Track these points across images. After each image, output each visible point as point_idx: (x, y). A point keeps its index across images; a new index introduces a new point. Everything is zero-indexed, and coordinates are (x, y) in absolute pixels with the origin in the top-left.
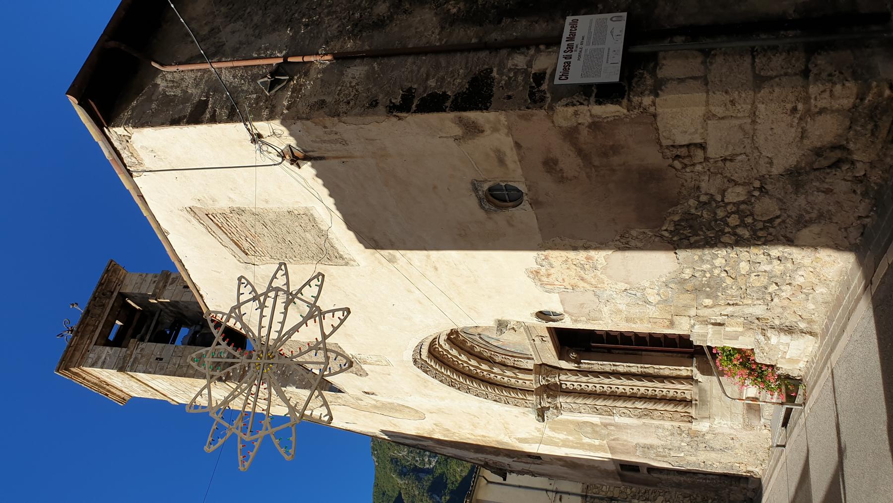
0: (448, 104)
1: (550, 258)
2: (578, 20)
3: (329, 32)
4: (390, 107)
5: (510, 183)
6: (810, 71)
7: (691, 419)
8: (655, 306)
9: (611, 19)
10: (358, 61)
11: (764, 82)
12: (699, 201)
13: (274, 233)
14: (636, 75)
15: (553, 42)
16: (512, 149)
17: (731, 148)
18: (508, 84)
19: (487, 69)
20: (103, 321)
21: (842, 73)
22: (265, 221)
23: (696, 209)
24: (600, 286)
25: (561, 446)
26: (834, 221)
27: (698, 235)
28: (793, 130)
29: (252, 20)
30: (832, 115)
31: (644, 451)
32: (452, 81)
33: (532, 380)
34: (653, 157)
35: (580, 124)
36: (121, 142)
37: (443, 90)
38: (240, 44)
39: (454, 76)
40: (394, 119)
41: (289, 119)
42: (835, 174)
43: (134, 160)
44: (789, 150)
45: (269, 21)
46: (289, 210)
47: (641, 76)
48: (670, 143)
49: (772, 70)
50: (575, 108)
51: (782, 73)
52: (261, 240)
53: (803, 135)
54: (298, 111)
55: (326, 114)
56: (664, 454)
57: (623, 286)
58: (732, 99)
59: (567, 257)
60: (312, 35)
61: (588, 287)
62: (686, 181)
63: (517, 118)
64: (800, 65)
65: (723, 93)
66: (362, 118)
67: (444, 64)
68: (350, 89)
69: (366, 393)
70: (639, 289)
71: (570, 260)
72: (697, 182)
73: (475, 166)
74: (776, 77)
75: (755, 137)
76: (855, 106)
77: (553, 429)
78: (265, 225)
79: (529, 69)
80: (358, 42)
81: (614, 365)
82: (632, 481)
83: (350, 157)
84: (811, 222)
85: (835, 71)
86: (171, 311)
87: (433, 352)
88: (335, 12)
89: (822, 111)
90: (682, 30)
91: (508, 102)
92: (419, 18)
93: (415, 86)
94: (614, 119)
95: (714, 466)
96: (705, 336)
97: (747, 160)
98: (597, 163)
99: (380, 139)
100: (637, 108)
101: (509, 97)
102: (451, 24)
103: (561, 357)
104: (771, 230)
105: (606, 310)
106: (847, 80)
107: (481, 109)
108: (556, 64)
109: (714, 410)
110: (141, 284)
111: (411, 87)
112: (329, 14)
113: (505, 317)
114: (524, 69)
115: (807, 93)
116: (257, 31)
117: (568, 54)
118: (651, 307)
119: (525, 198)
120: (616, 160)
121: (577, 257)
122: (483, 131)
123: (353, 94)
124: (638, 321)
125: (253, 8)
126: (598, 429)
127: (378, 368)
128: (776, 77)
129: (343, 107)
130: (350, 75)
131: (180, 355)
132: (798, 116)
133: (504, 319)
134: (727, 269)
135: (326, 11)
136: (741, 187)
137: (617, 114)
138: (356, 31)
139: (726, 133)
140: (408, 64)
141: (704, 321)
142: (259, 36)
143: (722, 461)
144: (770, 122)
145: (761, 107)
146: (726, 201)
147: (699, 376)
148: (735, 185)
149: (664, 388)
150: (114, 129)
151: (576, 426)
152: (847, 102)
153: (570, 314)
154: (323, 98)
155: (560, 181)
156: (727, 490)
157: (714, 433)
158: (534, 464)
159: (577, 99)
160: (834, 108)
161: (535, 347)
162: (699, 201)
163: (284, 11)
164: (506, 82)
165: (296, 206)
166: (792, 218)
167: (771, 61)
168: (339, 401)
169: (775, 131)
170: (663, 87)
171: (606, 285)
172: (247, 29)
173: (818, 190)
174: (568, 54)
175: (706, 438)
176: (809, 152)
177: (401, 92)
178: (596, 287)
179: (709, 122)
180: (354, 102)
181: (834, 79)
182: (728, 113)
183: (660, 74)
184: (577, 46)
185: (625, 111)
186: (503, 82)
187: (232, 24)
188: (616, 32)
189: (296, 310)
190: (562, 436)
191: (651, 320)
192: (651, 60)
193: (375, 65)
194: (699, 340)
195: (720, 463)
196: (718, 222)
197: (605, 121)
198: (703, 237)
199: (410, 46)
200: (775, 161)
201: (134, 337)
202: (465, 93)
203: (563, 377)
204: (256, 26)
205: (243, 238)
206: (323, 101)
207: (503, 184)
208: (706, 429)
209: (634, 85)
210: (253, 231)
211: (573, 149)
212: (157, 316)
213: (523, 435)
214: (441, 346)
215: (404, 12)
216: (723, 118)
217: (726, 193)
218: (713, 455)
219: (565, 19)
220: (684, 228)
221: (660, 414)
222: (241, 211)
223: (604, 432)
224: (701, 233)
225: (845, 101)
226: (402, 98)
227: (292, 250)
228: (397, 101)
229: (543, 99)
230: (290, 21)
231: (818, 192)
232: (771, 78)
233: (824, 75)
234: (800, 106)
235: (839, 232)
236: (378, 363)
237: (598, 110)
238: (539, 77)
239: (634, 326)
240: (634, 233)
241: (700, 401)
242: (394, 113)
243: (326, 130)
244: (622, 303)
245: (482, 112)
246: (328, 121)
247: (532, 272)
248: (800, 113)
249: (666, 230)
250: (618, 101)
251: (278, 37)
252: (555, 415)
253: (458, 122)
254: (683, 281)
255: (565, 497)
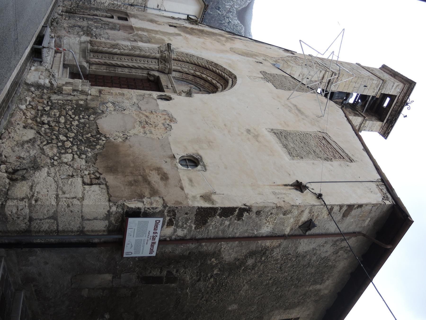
0: (219, 212)
1: (164, 128)
2: (149, 254)
3: (278, 250)
4: (250, 211)
5: (186, 169)
6: (28, 221)
7: (91, 42)
8: (109, 101)
9: (132, 253)
10: (264, 235)
11: (52, 216)
12: (86, 155)
13: (310, 147)
14: (119, 223)
15: (162, 241)
16: (185, 186)
17: (69, 182)
18: (187, 220)
19: (197, 229)
20: (392, 108)
21: (12, 219)
22: (314, 154)
23: (87, 151)
24: (138, 113)
25: (159, 31)
26: (15, 142)
27: (86, 137)
28: (37, 190)
29: (317, 258)
30: (17, 197)
31: (115, 27)
32: (216, 224)
33: (174, 66)
34: (110, 179)
35: (149, 198)
36: (387, 197)
37: (221, 219)
38: (324, 246)
39: (215, 226)
40: (248, 204)
41: (303, 206)
42: (15, 166)
43: (381, 187)
44: (39, 180)
45: (308, 257)
46: (302, 159)
47: (116, 221)
48: (102, 186)
49: (48, 222)
50: (152, 206)
51: (43, 221)
52: (316, 144)
53: (31, 188)
54: (298, 210)
55: (283, 208)
56: (105, 25)
57: (126, 112)
58: (69, 208)
59: (155, 128)
60: (287, 249)
61: (144, 112)
62: (93, 166)
63: (183, 202)
64: (34, 224)
65: (73, 211)
66: (265, 205)
67: (220, 232)
68: (270, 221)
69: (261, 63)
70: (117, 111)
71: (154, 127)
72: (87, 165)
73: (205, 178)
74: (46, 219)
75: (57, 187)
76: (6, 201)
77: (163, 40)
78: (314, 152)
79: (175, 228)
80: (264, 245)
81: (130, 72)
82: (122, 12)
83: (271, 185)
84: (28, 142)
85: (16, 220)
86: (358, 111)
87: (226, 82)
88: (274, 261)
89: (22, 199)
90: (94, 245)
91: (188, 211)
92: (231, 256)
93: (236, 221)
94: (131, 200)
95: (79, 18)
96: (83, 85)
97: (61, 176)
98: (140, 177)
99: (256, 194)
100: (119, 205)
101: (186, 214)
102: (215, 252)
103: (158, 77)
104: (48, 139)
105: (135, 100)
106: (10, 215)
107: (202, 208)
108: (161, 230)
109: (78, 47)
110: (372, 126)
111: (238, 221)
112: (277, 260)
113: (188, 98)
114: (178, 228)
115: (30, 209)
116: (315, 252)
117: (155, 235)
118: (111, 101)
119: (178, 161)
120: (130, 179)
121: (150, 128)
122: (201, 196)
123: (269, 218)
124: (118, 94)
125: (315, 264)
126: (139, 39)
127: (255, 75)
128: (46, 219)
129: (274, 211)
130: (269, 228)
131: (355, 88)
132: (34, 197)
133: (189, 97)
134: (71, 119)
135: (279, 261)
136: (64, 162)
137: (129, 202)
138: (264, 250)
139: (72, 190)
140: (238, 233)
141: (83, 92)
142: (314, 249)
143: (75, 21)
144: (49, 195)
145: (54, 203)
146: (72, 155)
147: (85, 65)
148: (67, 163)
149: (104, 59)
150: (390, 203)
151: (151, 41)
152: (10, 203)
153: (153, 98)
154: (284, 217)
155: (159, 169)
156: (72, 6)
157: (78, 35)
158: (172, 23)
159: (151, 211)
160: (16, 200)
161: (172, 83)
162: (86, 155)
163: (300, 262)
164: (188, 222)
165: (299, 161)
166: (37, 144)
167: (48, 227)
168: (275, 60)
169: (46, 190)
170: (105, 215)
171: (135, 113)
172: (319, 253)
173: (24, 159)
174: (155, 235)
175: (83, 33)
176: (29, 178)
177: (243, 219)
178: (140, 112)
179: (81, 196)
180: (269, 214)
181: (16, 216)
182: (71, 200)
183: (107, 222)
184: (150, 239)
185: (125, 204)
186: (189, 222)
187: (327, 256)
188: (129, 246)
189: (298, 107)
190: (158, 36)
191: (111, 94)
192: (110, 231)
193: (256, 233)
194: (86, 83)
195: (76, 20)
196: (76, 144)
197: (136, 199)
198: (84, 136)
199: (237, 242)
200: (46, 174)
201: (377, 98)
202: (210, 217)
203: (157, 67)
204: (315, 254)
205: (325, 146)
206: (284, 214)
207: (189, 168)
208: (82, 37)
209: (120, 218)
210: (321, 149)
211: (153, 185)
212: (365, 109)
213: (179, 38)
214: (221, 85)
215: (239, 260)
216: (73, 198)
217: (72, 159)
218: (79, 24)
219: (156, 254)
220: (94, 141)
221: (107, 46)
222: (326, 159)
223: (136, 38)
224: (85, 138)
225: (10, 204)
226: (243, 215)
227: (301, 138)
228: (245, 214)
229: (169, 212)
230: (297, 257)
231: (24, 157)
232: (48, 218)
233: (21, 218)
234: (33, 202)
235: (13, 136)
236: (255, 78)
237: (140, 205)
238: (170, 223)
239: (120, 91)
240: (120, 140)
241: (85, 52)
242: (248, 207)
243: (283, 200)
244: (127, 104)
245: (201, 206)
246: (282, 204)
247: (174, 121)
248: (33, 199)
249: (103, 140)
250: (129, 209)
251: (305, 248)
252: (162, 47)
253: (214, 202)
254: (95, 113)
255: (156, 7)
